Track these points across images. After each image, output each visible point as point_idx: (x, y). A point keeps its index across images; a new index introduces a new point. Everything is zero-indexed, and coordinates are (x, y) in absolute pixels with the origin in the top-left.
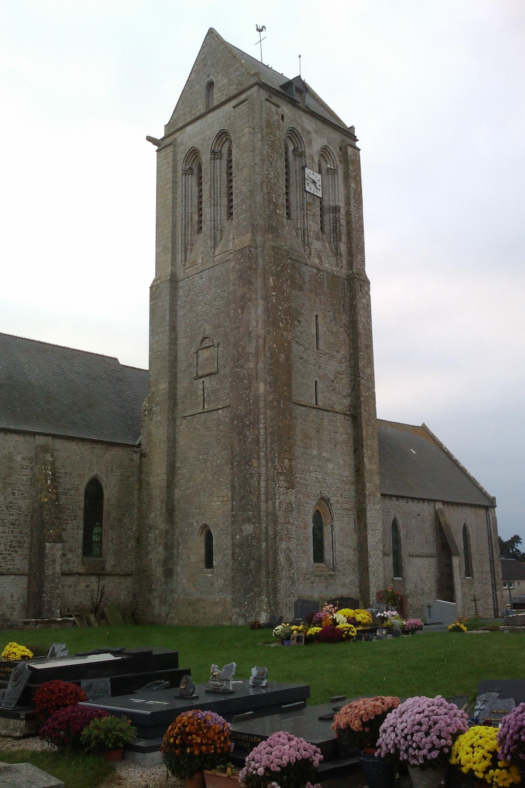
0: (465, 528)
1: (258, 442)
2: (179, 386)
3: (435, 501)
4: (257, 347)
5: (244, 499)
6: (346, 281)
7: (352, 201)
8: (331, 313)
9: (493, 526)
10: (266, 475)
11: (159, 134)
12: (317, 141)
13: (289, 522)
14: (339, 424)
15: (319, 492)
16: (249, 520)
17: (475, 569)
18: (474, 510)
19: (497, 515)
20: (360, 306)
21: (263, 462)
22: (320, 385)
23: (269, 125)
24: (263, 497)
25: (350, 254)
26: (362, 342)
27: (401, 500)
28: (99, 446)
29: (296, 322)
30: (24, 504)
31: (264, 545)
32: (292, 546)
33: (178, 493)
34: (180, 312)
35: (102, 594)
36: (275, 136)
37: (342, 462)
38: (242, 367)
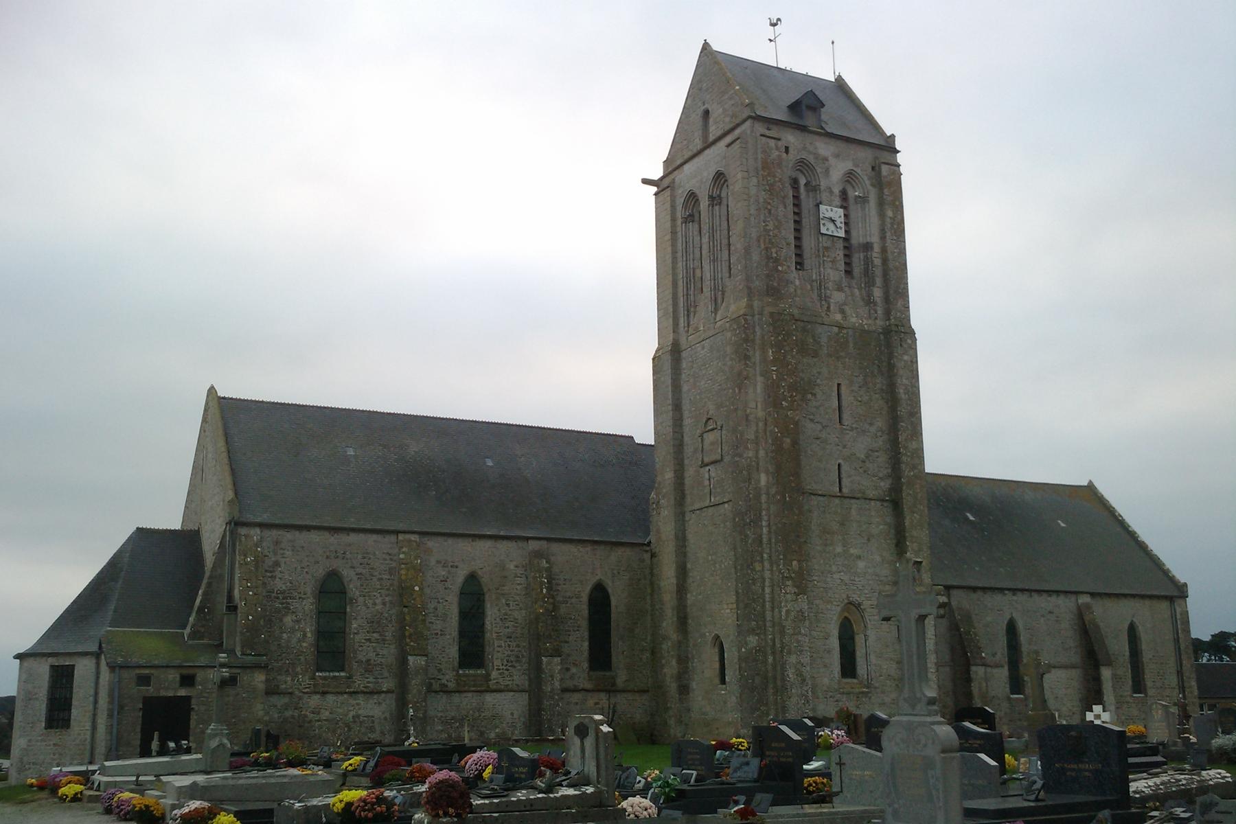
0: (1132, 630)
1: (761, 542)
2: (687, 475)
3: (1076, 593)
4: (757, 431)
5: (751, 610)
6: (882, 337)
7: (888, 234)
8: (861, 377)
9: (1182, 623)
10: (771, 579)
11: (657, 173)
12: (837, 167)
13: (800, 633)
14: (873, 513)
15: (844, 596)
16: (752, 631)
17: (1149, 684)
18: (1147, 602)
19: (1189, 609)
20: (900, 365)
21: (767, 564)
22: (845, 468)
23: (766, 165)
24: (768, 605)
25: (887, 299)
26: (903, 411)
27: (1019, 594)
28: (602, 547)
29: (809, 396)
30: (520, 615)
31: (770, 659)
32: (806, 659)
33: (690, 599)
34: (685, 388)
35: (614, 712)
36: (774, 176)
37: (878, 558)
38: (740, 456)
